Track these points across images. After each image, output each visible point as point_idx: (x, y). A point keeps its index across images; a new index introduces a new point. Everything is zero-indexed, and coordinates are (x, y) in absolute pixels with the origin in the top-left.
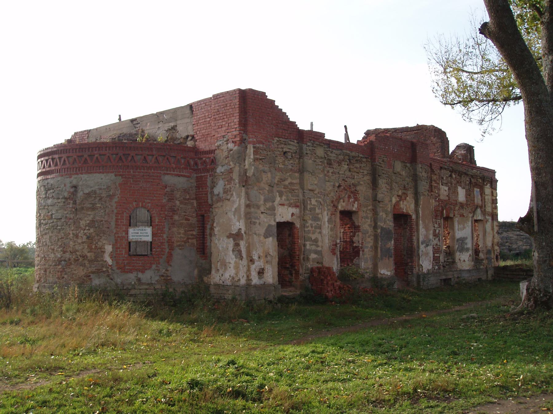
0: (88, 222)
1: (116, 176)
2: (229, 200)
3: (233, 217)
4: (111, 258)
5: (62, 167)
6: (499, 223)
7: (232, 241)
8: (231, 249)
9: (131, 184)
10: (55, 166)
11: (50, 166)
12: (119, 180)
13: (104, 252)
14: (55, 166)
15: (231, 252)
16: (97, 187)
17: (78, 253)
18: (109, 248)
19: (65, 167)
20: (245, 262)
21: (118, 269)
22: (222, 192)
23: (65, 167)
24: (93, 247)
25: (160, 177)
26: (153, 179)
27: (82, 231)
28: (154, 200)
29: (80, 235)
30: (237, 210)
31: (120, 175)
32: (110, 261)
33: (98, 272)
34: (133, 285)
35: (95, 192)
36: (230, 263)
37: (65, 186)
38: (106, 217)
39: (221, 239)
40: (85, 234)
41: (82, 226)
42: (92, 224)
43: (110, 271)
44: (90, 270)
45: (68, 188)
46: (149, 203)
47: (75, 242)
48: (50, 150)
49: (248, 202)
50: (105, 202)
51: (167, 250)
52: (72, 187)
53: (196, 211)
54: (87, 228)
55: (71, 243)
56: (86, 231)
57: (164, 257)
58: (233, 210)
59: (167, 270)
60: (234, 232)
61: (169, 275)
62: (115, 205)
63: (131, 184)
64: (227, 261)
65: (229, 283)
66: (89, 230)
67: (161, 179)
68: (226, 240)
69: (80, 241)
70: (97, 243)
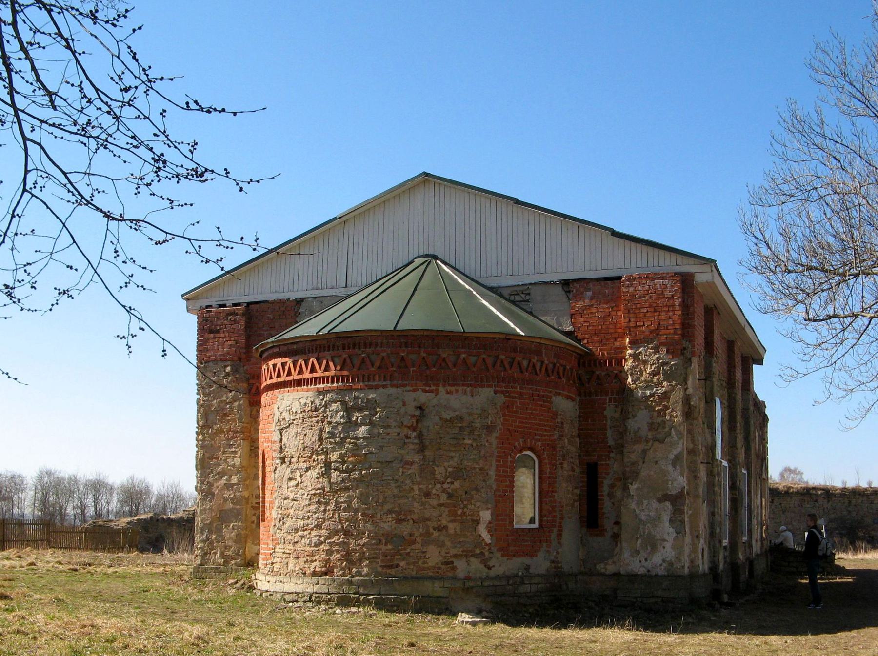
0: (450, 469)
1: (495, 392)
2: (661, 441)
3: (670, 468)
4: (489, 531)
5: (339, 373)
6: (775, 492)
7: (670, 507)
8: (666, 517)
9: (517, 407)
10: (311, 372)
11: (289, 374)
12: (501, 399)
13: (478, 522)
14: (311, 372)
15: (667, 524)
16: (464, 410)
17: (429, 523)
18: (486, 515)
19: (327, 374)
20: (688, 539)
21: (498, 550)
22: (645, 427)
23: (327, 374)
24: (459, 512)
25: (551, 397)
26: (544, 401)
27: (438, 486)
28: (545, 436)
29: (434, 491)
30: (677, 459)
31: (502, 392)
32: (487, 538)
33: (467, 555)
34: (522, 578)
35: (461, 419)
36: (664, 540)
37: (404, 404)
38: (481, 461)
39: (645, 502)
40: (444, 491)
41: (439, 477)
42: (457, 474)
43: (487, 553)
44: (453, 552)
45: (411, 409)
46: (539, 441)
47: (423, 504)
48: (491, 336)
49: (691, 446)
50: (480, 436)
51: (558, 520)
52: (417, 408)
53: (579, 456)
54: (449, 480)
55: (416, 505)
56: (446, 486)
57: (555, 530)
58: (672, 456)
59: (558, 553)
60: (674, 492)
61: (559, 560)
62: (495, 443)
63: (517, 407)
64: (658, 537)
65: (661, 572)
66: (452, 483)
67: (552, 403)
68: (655, 504)
69: (434, 502)
70: (465, 506)
